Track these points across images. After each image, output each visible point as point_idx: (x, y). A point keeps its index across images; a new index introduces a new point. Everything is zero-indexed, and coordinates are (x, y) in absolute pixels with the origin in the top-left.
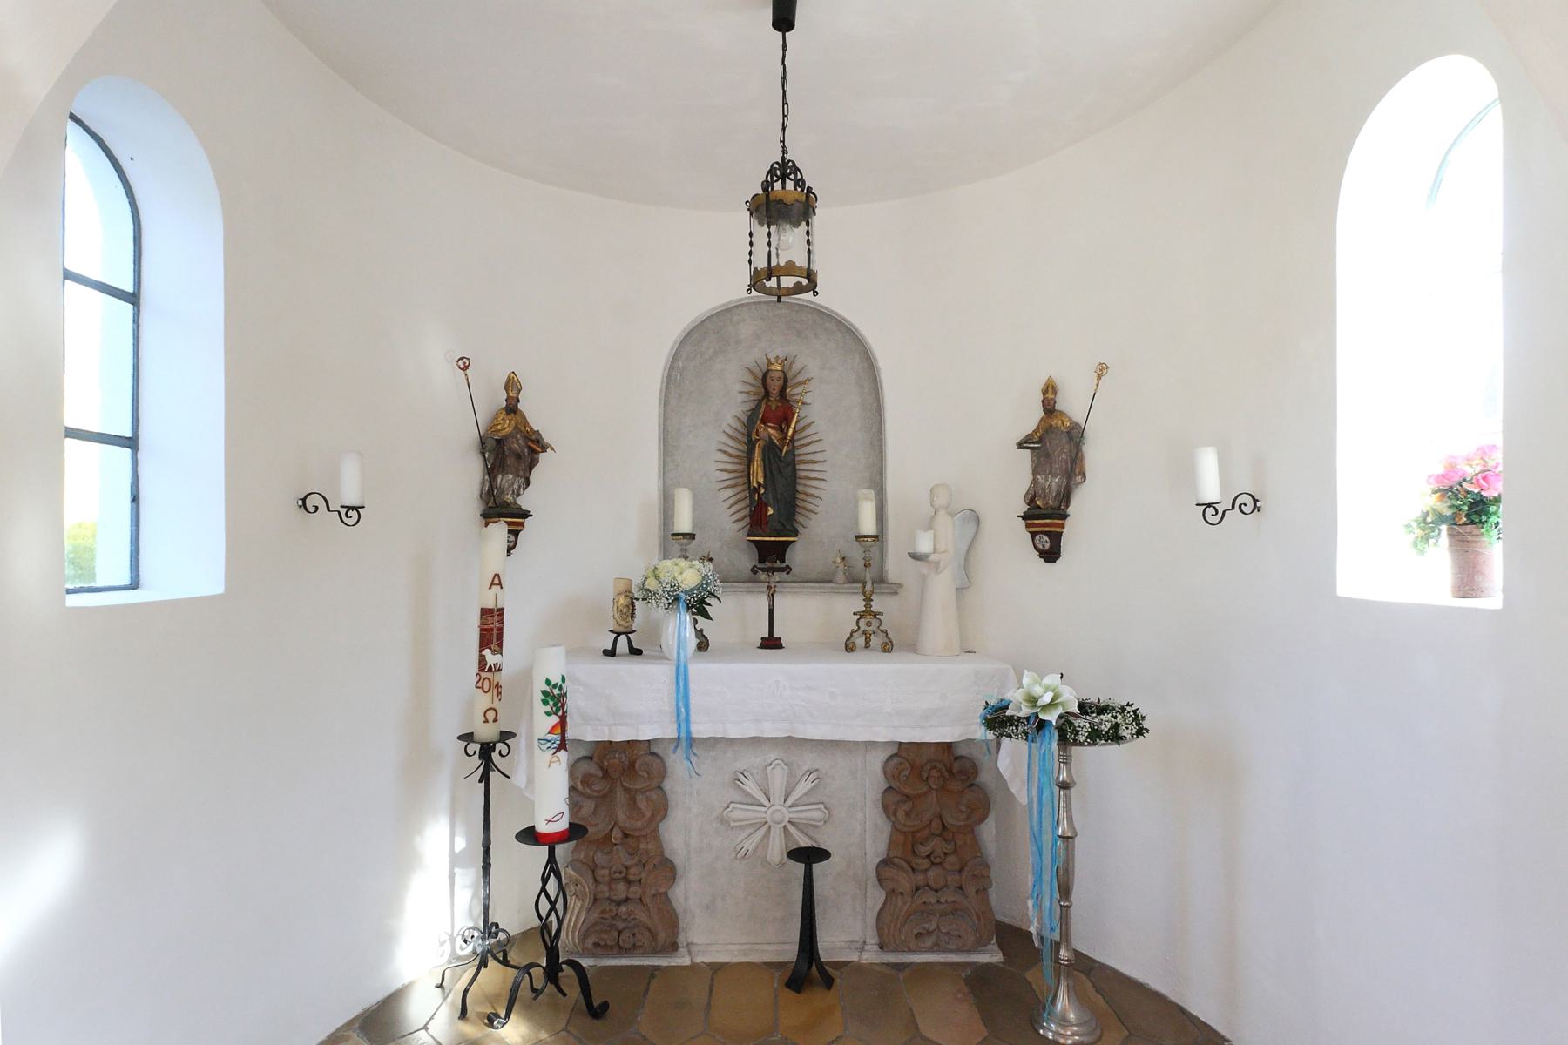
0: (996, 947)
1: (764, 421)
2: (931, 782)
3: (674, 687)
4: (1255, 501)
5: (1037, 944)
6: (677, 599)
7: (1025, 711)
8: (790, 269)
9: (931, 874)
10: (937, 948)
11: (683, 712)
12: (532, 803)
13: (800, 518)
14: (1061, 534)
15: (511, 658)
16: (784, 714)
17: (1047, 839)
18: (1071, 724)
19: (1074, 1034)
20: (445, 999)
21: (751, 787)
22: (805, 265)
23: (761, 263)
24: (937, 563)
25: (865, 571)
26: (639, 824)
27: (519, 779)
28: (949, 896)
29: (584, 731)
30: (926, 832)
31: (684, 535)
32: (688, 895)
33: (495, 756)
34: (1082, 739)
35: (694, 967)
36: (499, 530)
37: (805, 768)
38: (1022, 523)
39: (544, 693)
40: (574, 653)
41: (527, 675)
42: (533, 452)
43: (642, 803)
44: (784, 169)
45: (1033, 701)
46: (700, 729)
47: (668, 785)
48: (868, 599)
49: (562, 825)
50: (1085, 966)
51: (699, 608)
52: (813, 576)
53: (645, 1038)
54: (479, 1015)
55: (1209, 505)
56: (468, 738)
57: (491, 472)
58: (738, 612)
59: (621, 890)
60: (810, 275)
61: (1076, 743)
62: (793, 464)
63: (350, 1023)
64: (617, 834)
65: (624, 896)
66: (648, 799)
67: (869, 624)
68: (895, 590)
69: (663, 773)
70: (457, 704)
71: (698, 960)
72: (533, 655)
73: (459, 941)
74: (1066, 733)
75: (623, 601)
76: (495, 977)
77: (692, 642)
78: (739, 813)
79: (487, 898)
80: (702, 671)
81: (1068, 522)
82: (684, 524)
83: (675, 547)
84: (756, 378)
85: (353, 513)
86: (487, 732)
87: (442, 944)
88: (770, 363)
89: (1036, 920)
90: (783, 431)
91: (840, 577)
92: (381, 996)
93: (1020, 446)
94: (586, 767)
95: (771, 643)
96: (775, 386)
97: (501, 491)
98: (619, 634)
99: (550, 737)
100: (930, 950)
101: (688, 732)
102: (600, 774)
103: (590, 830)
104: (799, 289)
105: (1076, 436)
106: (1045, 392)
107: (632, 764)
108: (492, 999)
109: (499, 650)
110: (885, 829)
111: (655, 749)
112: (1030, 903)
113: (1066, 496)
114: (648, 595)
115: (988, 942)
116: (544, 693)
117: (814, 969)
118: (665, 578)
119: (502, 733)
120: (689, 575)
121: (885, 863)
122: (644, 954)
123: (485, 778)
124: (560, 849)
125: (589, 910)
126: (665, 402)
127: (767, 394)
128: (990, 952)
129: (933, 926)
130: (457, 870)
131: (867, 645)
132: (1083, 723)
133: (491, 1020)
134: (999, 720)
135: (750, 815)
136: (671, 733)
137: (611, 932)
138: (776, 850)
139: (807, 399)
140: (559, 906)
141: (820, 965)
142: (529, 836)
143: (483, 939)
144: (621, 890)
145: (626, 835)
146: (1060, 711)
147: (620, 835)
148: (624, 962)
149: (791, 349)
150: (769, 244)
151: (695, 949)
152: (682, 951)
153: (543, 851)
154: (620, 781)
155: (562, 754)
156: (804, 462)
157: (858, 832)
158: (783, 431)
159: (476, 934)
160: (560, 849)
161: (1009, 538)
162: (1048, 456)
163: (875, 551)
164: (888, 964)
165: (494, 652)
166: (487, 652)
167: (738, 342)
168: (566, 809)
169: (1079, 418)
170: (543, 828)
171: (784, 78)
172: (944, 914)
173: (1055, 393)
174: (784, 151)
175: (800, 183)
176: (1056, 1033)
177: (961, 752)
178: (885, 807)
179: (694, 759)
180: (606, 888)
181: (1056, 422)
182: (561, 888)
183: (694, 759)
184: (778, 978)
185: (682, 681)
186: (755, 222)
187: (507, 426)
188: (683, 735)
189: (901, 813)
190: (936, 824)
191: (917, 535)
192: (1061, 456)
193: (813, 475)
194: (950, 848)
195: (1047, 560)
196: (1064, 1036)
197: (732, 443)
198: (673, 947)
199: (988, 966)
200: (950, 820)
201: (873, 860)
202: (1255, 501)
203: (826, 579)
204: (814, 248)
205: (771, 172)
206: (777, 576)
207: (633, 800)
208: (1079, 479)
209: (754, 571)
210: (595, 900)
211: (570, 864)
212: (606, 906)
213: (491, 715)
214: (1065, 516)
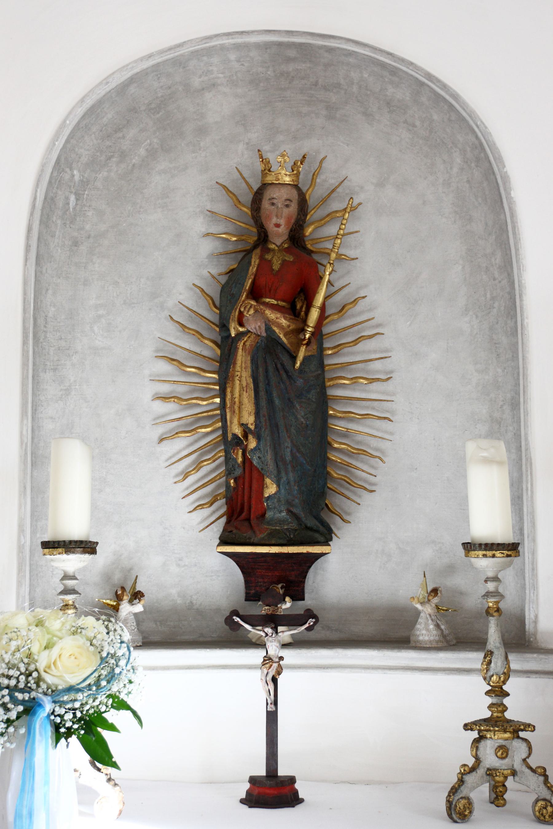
1: (255, 294)
48: (498, 692)
67: (503, 751)
96: (279, 228)
131: (498, 797)
167: (202, 131)
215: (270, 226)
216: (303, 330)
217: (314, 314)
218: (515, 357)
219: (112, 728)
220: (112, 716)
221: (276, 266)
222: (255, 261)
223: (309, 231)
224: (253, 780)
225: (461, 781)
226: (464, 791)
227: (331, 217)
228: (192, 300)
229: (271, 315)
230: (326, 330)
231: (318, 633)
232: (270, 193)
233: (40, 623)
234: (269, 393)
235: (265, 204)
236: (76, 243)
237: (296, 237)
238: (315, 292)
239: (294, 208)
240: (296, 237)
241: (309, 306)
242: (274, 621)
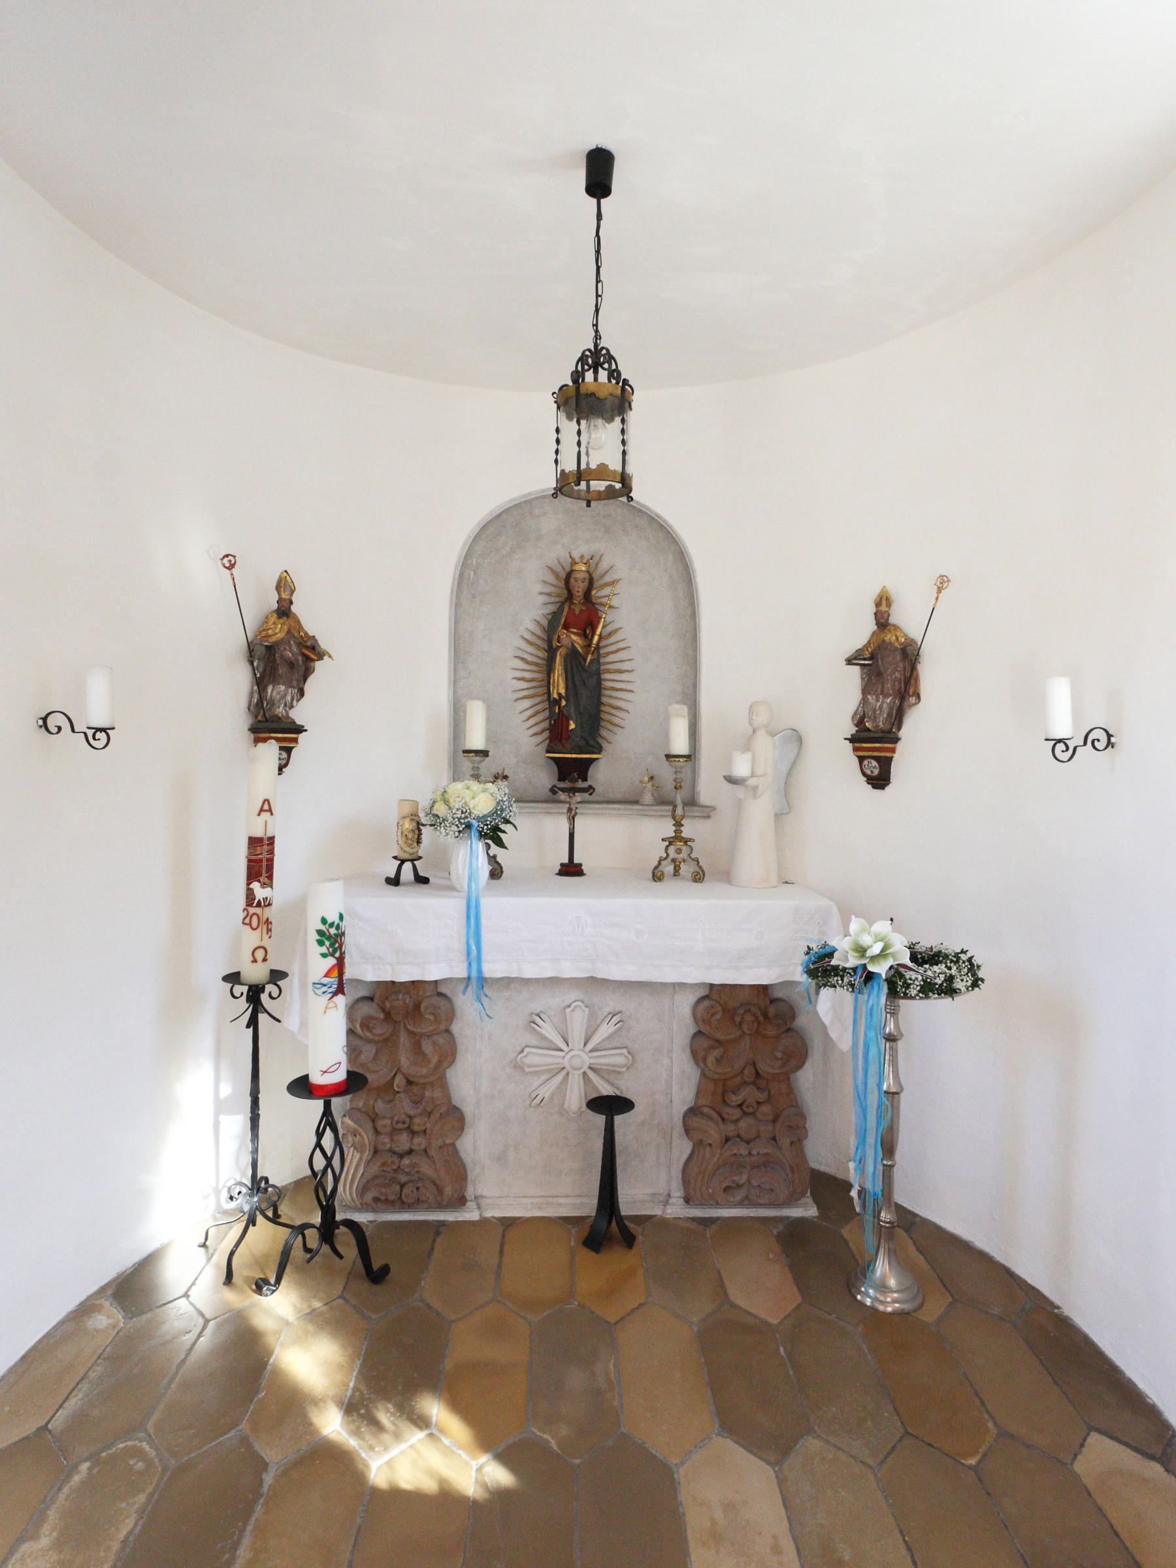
0: (810, 1200)
1: (566, 626)
2: (745, 1027)
3: (464, 922)
4: (1109, 736)
5: (858, 1209)
6: (469, 826)
7: (852, 961)
8: (602, 472)
9: (743, 1124)
10: (747, 1202)
12: (306, 1047)
13: (604, 733)
14: (890, 759)
15: (284, 887)
16: (580, 950)
17: (873, 1099)
18: (901, 976)
19: (895, 1301)
20: (209, 1259)
21: (548, 1030)
22: (620, 470)
23: (570, 465)
24: (756, 788)
25: (674, 793)
26: (424, 1071)
27: (292, 1022)
28: (761, 1148)
29: (367, 968)
30: (738, 1080)
31: (477, 752)
32: (476, 1145)
33: (264, 998)
34: (914, 993)
35: (484, 1221)
36: (270, 751)
37: (606, 1010)
38: (849, 746)
39: (320, 932)
41: (300, 906)
42: (308, 659)
44: (597, 357)
45: (861, 951)
46: (493, 969)
47: (455, 1028)
48: (678, 825)
49: (340, 1076)
50: (909, 1222)
51: (493, 834)
52: (619, 796)
53: (429, 1307)
54: (247, 1280)
55: (1060, 741)
56: (233, 978)
57: (261, 682)
58: (537, 836)
59: (404, 1142)
60: (625, 479)
61: (906, 996)
62: (597, 675)
63: (102, 1290)
64: (399, 1082)
65: (406, 1147)
66: (434, 1044)
67: (679, 851)
68: (707, 812)
69: (451, 1015)
70: (221, 939)
71: (488, 1214)
73: (225, 1195)
74: (896, 985)
75: (408, 825)
76: (265, 1236)
77: (484, 868)
78: (536, 1058)
79: (255, 1151)
80: (498, 906)
81: (900, 746)
82: (476, 739)
83: (466, 764)
84: (558, 577)
85: (102, 736)
86: (255, 973)
87: (206, 1197)
88: (574, 563)
89: (860, 1175)
90: (587, 638)
91: (648, 798)
92: (137, 1258)
93: (849, 662)
94: (367, 1009)
95: (571, 869)
96: (579, 588)
97: (272, 703)
98: (403, 862)
99: (326, 980)
101: (480, 971)
102: (382, 1016)
103: (370, 1077)
104: (610, 494)
105: (910, 655)
106: (878, 604)
107: (417, 1006)
108: (259, 1262)
109: (269, 882)
111: (443, 990)
112: (852, 1165)
113: (898, 717)
114: (437, 822)
115: (803, 1195)
116: (320, 932)
117: (614, 1224)
118: (456, 804)
119: (272, 972)
120: (481, 800)
122: (430, 1208)
123: (253, 1023)
124: (336, 1102)
125: (369, 1162)
126: (457, 605)
127: (570, 596)
128: (804, 1206)
129: (744, 1178)
130: (222, 1118)
131: (676, 872)
132: (915, 976)
133: (260, 1286)
134: (822, 968)
135: (551, 1060)
136: (460, 972)
137: (393, 1183)
138: (575, 1098)
139: (615, 602)
140: (336, 1162)
141: (621, 1220)
142: (302, 1087)
143: (251, 1196)
144: (404, 1142)
145: (410, 1083)
146: (890, 962)
147: (404, 1082)
149: (596, 547)
150: (579, 443)
151: (483, 1202)
152: (471, 1204)
154: (402, 1024)
155: (340, 1000)
156: (609, 671)
157: (665, 1079)
158: (587, 638)
159: (244, 1190)
160: (336, 1102)
161: (834, 762)
162: (880, 674)
163: (687, 770)
164: (694, 1219)
165: (264, 885)
166: (255, 885)
168: (343, 1058)
169: (915, 633)
170: (317, 1079)
171: (598, 252)
172: (755, 1167)
173: (889, 605)
174: (597, 336)
175: (614, 374)
176: (875, 1299)
177: (778, 994)
178: (694, 1054)
179: (485, 1000)
180: (387, 1140)
181: (889, 637)
182: (338, 1143)
183: (485, 1000)
184: (574, 1237)
186: (562, 416)
187: (278, 631)
188: (474, 974)
189: (711, 1060)
190: (749, 1071)
191: (735, 761)
192: (893, 674)
193: (619, 685)
194: (762, 1097)
195: (875, 787)
196: (882, 1302)
197: (530, 649)
198: (460, 1201)
199: (801, 1221)
200: (764, 1068)
202: (1109, 736)
203: (631, 801)
204: (630, 448)
205: (582, 359)
206: (578, 797)
207: (417, 1049)
208: (913, 700)
209: (553, 790)
210: (376, 1152)
211: (348, 1113)
212: (388, 1158)
213: (260, 953)
214: (896, 740)
215: (575, 592)
216: (590, 646)
217: (596, 638)
218: (695, 663)
219: (504, 832)
220: (502, 826)
221: (577, 612)
222: (566, 609)
223: (593, 592)
224: (562, 865)
225: (659, 863)
226: (661, 868)
227: (607, 585)
228: (532, 627)
229: (574, 637)
230: (601, 644)
231: (594, 797)
232: (574, 575)
233: (468, 788)
234: (573, 677)
235: (572, 581)
236: (474, 597)
237: (587, 594)
238: (597, 627)
239: (586, 583)
240: (587, 594)
241: (593, 634)
242: (573, 791)
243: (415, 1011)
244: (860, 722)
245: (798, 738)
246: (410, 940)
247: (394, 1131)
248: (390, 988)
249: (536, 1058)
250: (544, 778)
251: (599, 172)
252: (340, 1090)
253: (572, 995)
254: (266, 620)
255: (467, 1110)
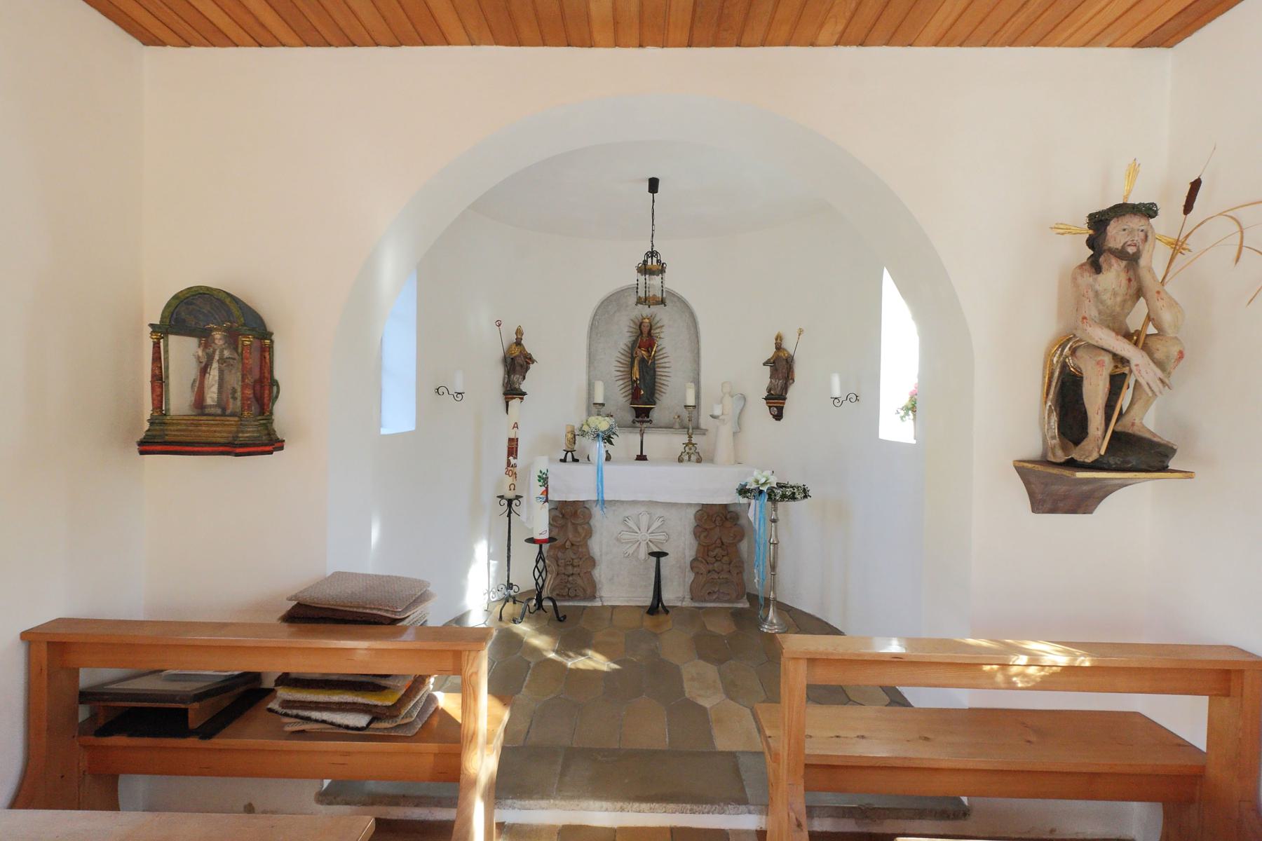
7: (754, 486)
10: (718, 600)
11: (600, 490)
15: (520, 461)
16: (647, 495)
21: (631, 524)
25: (689, 423)
27: (523, 517)
32: (601, 574)
35: (603, 606)
40: (551, 460)
43: (580, 529)
44: (652, 254)
45: (757, 482)
47: (592, 522)
48: (690, 437)
49: (546, 536)
51: (608, 439)
58: (627, 442)
68: (704, 432)
69: (590, 516)
72: (534, 460)
75: (570, 436)
78: (626, 536)
80: (608, 468)
82: (599, 399)
83: (594, 410)
86: (510, 495)
90: (649, 352)
91: (677, 426)
93: (764, 364)
95: (641, 457)
96: (645, 330)
100: (714, 601)
105: (529, 360)
110: (695, 544)
113: (785, 388)
114: (583, 434)
120: (603, 424)
121: (695, 560)
123: (509, 516)
126: (590, 337)
138: (643, 553)
140: (544, 574)
142: (531, 540)
144: (570, 570)
148: (571, 604)
153: (537, 546)
154: (570, 518)
157: (682, 546)
161: (759, 409)
163: (695, 413)
170: (537, 537)
177: (732, 509)
178: (695, 534)
185: (600, 472)
187: (516, 352)
198: (593, 597)
201: (689, 559)
203: (669, 427)
207: (576, 530)
213: (513, 487)
243: (575, 514)
244: (769, 390)
245: (744, 398)
246: (575, 484)
247: (566, 565)
248: (564, 504)
249: (626, 536)
250: (629, 416)
251: (653, 185)
252: (545, 541)
253: (642, 509)
254: (510, 347)
255: (597, 557)
